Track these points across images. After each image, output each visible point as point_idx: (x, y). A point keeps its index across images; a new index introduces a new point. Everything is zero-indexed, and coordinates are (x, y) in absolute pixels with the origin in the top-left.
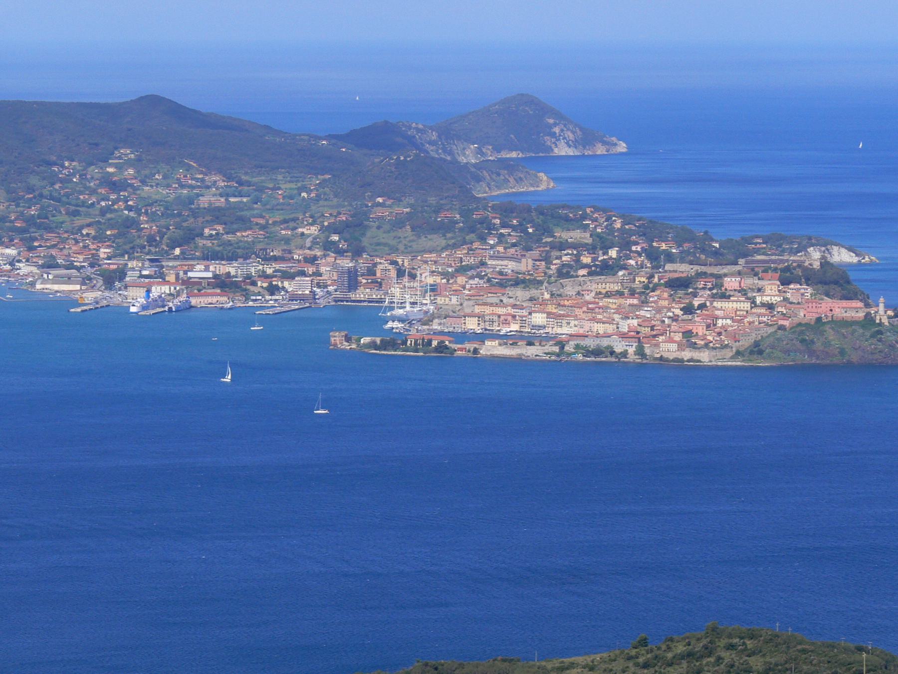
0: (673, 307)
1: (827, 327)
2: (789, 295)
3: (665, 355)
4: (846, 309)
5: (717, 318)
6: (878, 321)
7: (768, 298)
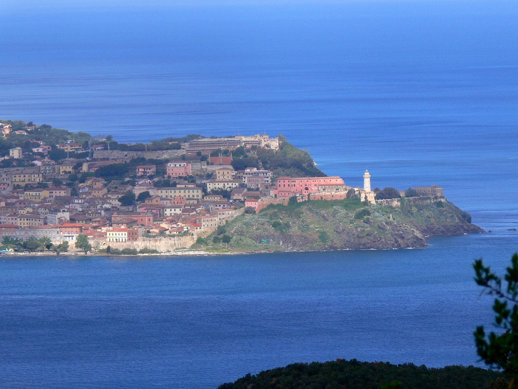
0: (109, 198)
1: (304, 209)
2: (246, 181)
3: (114, 246)
4: (325, 187)
5: (164, 208)
6: (363, 200)
7: (221, 185)
